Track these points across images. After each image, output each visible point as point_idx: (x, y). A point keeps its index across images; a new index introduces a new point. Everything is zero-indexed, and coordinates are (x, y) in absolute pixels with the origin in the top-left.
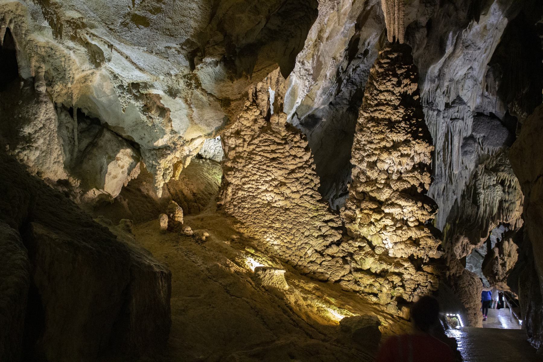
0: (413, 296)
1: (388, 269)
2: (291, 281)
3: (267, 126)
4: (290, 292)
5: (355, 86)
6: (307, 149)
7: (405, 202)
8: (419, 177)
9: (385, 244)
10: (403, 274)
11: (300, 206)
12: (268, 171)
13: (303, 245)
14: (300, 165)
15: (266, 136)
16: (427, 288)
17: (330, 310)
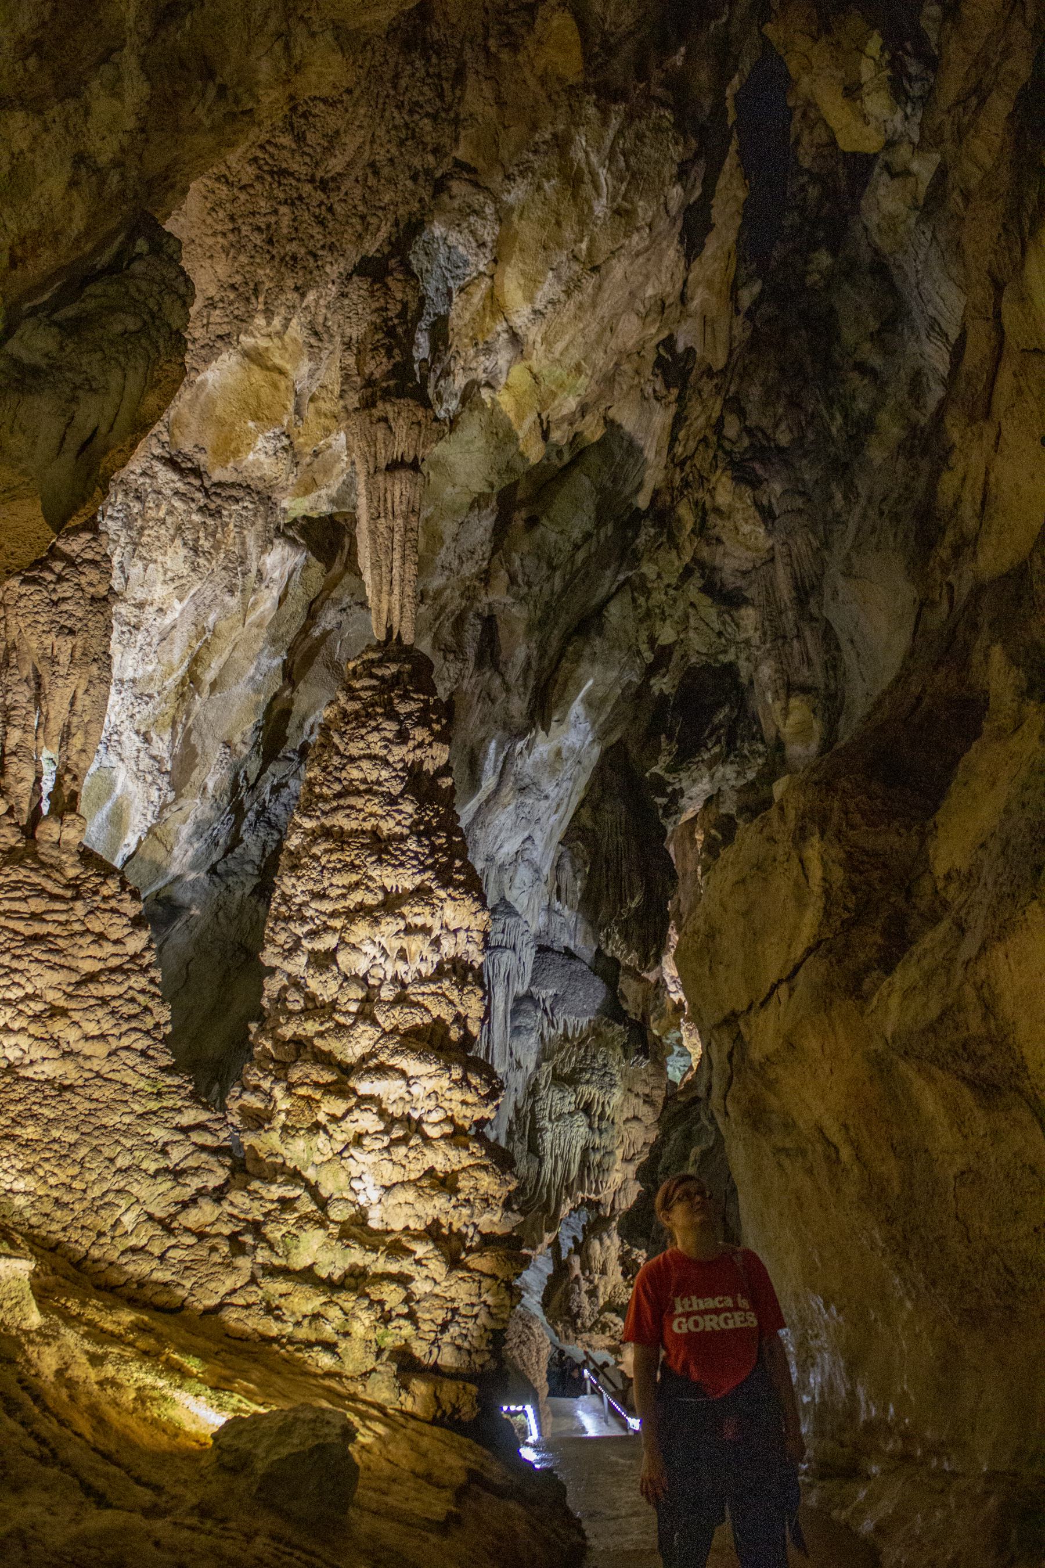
0: (439, 1347)
1: (365, 1267)
2: (58, 1301)
3: (24, 849)
4: (46, 1336)
5: (275, 833)
6: (137, 922)
7: (417, 1063)
8: (454, 995)
9: (357, 1194)
10: (410, 1279)
11: (106, 1079)
12: (16, 971)
13: (110, 1197)
14: (114, 962)
15: (21, 874)
16: (479, 1322)
17: (184, 1398)
